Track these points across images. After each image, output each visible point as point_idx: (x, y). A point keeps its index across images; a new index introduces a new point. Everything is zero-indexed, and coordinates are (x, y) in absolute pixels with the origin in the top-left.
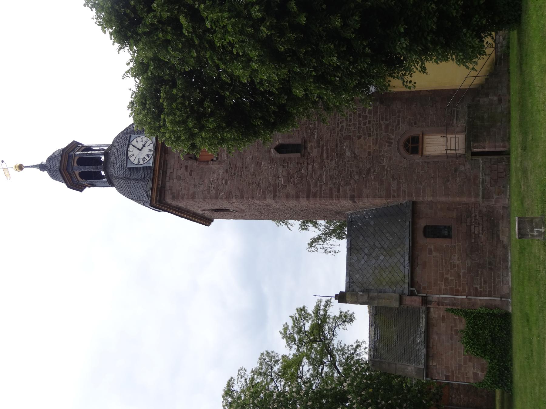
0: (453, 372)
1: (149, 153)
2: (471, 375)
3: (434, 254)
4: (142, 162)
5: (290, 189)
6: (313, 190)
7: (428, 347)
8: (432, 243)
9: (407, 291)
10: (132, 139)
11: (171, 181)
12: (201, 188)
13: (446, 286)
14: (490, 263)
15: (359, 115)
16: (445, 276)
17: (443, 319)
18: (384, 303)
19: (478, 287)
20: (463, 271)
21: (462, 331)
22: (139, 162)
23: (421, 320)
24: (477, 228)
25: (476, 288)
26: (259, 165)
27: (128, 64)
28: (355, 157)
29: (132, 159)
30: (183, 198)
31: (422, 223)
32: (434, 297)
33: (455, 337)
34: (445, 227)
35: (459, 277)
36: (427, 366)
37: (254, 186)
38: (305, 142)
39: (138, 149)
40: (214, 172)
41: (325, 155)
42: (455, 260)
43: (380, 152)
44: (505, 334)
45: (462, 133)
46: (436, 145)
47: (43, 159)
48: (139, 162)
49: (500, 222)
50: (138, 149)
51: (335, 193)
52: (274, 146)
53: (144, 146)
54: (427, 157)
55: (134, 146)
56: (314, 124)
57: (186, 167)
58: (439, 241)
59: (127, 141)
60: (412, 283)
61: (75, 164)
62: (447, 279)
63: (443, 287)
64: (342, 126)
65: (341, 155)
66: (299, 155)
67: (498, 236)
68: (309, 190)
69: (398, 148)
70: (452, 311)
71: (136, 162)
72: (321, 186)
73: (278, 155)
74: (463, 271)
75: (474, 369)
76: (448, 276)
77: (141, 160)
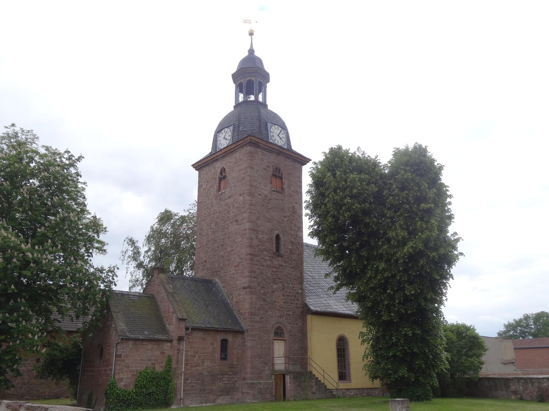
0: (124, 361)
2: (122, 376)
3: (211, 347)
4: (272, 134)
5: (255, 242)
6: (255, 259)
7: (143, 340)
8: (218, 345)
9: (188, 325)
11: (261, 153)
12: (256, 175)
13: (191, 355)
14: (204, 390)
15: (295, 296)
16: (197, 355)
17: (163, 353)
18: (166, 305)
19: (189, 381)
20: (200, 369)
21: (154, 369)
23: (161, 335)
24: (226, 379)
25: (188, 380)
26: (269, 221)
27: (358, 149)
28: (273, 292)
30: (251, 160)
31: (230, 338)
32: (184, 346)
33: (150, 362)
34: (226, 355)
35: (196, 366)
36: (128, 339)
37: (258, 215)
38: (282, 256)
40: (265, 186)
41: (274, 270)
42: (207, 363)
43: (276, 309)
44: (153, 404)
45: (285, 368)
46: (279, 349)
47: (256, 54)
49: (230, 397)
51: (253, 274)
52: (280, 234)
53: (281, 138)
54: (273, 343)
56: (291, 264)
57: (268, 167)
58: (218, 350)
60: (194, 329)
61: (259, 80)
62: (195, 356)
63: (190, 353)
64: (289, 284)
65: (274, 282)
66: (275, 251)
67: (221, 395)
68: (255, 255)
69: (277, 323)
70: (170, 360)
72: (257, 265)
73: (274, 236)
74: (200, 369)
75: (127, 378)
76: (197, 358)
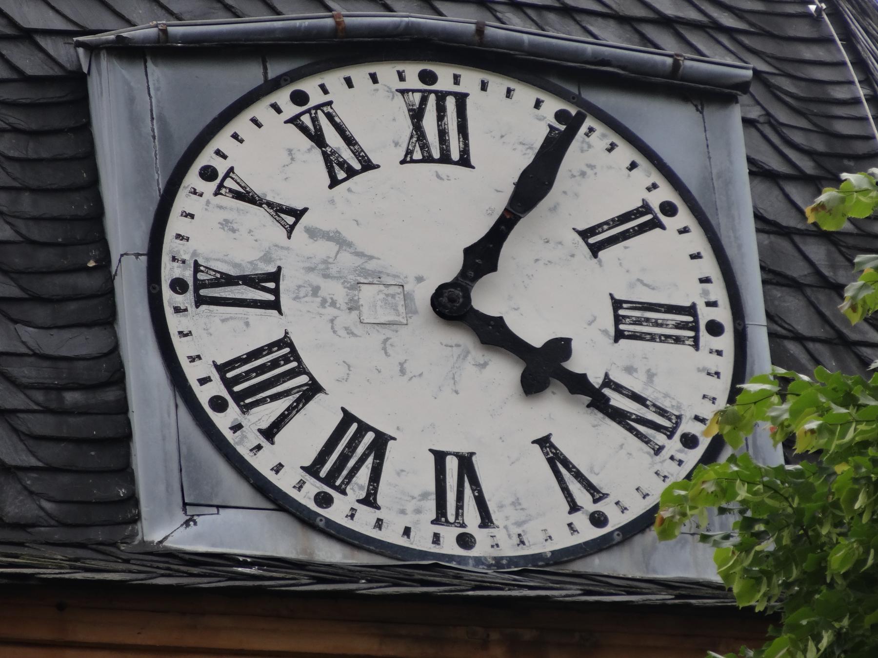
1: (407, 476)
10: (670, 125)
22: (211, 288)
29: (265, 148)
39: (482, 257)
48: (211, 288)
50: (482, 257)
53: (545, 368)
55: (533, 186)
59: (611, 42)
71: (208, 232)
77: (262, 328)
